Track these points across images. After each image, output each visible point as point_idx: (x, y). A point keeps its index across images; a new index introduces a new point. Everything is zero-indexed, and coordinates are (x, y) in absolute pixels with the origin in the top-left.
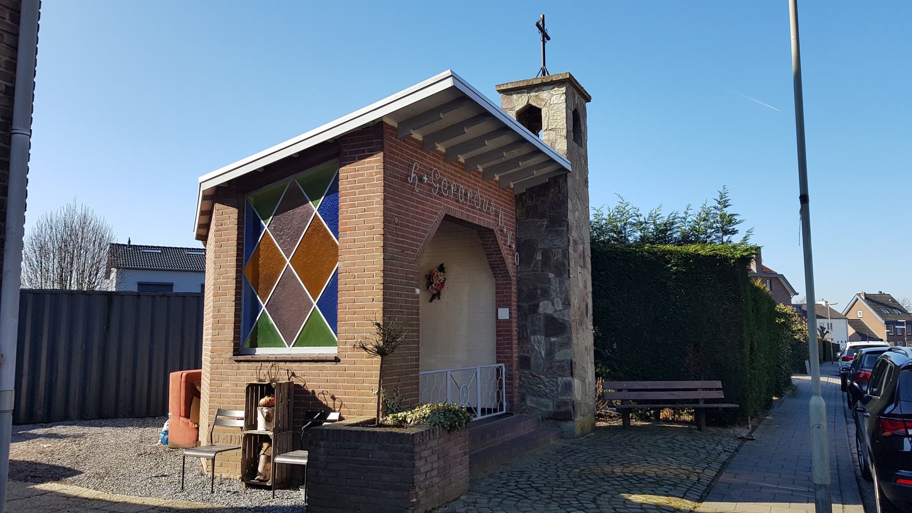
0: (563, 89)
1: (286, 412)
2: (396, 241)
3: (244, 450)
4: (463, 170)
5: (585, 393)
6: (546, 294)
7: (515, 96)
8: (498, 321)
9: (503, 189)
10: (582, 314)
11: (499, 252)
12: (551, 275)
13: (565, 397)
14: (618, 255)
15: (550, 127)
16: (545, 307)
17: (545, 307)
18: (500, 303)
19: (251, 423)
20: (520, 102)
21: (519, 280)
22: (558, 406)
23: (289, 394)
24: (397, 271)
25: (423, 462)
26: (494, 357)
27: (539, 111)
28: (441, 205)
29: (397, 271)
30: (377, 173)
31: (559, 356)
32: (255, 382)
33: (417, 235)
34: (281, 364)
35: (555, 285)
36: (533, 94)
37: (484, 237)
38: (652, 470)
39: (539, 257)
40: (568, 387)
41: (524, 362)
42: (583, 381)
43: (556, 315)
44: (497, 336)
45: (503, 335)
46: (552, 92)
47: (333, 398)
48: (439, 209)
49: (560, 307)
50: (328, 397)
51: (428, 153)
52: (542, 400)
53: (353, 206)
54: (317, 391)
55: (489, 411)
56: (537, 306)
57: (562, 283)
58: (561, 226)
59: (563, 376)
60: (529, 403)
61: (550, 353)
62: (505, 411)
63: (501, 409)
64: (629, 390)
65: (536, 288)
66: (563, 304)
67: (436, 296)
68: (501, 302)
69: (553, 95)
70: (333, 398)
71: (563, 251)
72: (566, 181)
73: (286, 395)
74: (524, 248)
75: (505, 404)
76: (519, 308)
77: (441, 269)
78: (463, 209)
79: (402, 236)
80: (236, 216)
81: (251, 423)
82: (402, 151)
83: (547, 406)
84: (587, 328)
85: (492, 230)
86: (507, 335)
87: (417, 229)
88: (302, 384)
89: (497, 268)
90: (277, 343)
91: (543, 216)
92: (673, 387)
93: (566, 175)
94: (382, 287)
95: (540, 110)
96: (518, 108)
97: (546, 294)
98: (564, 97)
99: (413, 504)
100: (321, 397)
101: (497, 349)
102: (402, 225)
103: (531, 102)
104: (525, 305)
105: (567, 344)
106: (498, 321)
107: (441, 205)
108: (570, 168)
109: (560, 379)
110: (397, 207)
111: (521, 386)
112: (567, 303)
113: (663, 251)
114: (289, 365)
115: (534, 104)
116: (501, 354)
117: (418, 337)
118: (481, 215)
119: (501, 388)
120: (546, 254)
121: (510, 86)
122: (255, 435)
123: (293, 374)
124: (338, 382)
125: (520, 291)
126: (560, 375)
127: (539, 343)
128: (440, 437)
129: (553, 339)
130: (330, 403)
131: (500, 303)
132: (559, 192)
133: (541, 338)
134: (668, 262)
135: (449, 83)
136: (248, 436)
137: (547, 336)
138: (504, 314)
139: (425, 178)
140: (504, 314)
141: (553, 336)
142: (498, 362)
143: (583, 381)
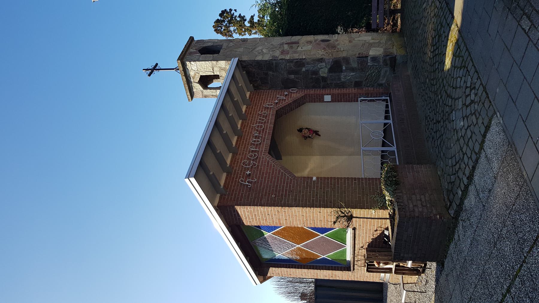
0: (188, 63)
1: (383, 253)
2: (285, 196)
3: (404, 274)
4: (241, 137)
5: (379, 44)
6: (316, 73)
7: (194, 90)
8: (332, 101)
9: (251, 101)
10: (328, 46)
11: (289, 105)
12: (304, 69)
15: (212, 70)
16: (324, 72)
17: (324, 72)
18: (321, 100)
19: (389, 270)
21: (307, 87)
22: (387, 65)
23: (373, 251)
24: (303, 196)
25: (416, 210)
26: (353, 104)
27: (202, 77)
28: (263, 158)
29: (303, 196)
30: (247, 209)
31: (355, 65)
32: (366, 268)
33: (281, 178)
34: (356, 252)
35: (310, 67)
36: (192, 80)
37: (281, 114)
38: (430, 33)
39: (292, 76)
40: (374, 59)
42: (371, 45)
43: (329, 67)
44: (341, 102)
45: (341, 98)
46: (190, 69)
47: (376, 230)
48: (266, 160)
49: (324, 64)
50: (375, 233)
51: (233, 168)
52: (382, 74)
53: (266, 220)
54: (372, 237)
55: (387, 112)
56: (323, 77)
57: (308, 64)
58: (273, 64)
59: (367, 62)
60: (384, 82)
61: (353, 70)
62: (388, 98)
63: (386, 101)
64: (378, 9)
66: (321, 62)
67: (317, 133)
68: (321, 99)
69: (192, 69)
70: (376, 230)
72: (244, 61)
73: (374, 253)
74: (287, 85)
75: (383, 98)
76: (324, 87)
77: (300, 130)
78: (264, 138)
79: (283, 192)
80: (274, 269)
81: (389, 270)
82: (233, 191)
83: (386, 71)
84: (337, 40)
85: (277, 111)
86: (341, 96)
87: (278, 177)
88: (367, 244)
89: (299, 103)
90: (344, 252)
94: (312, 208)
95: (201, 76)
96: (202, 89)
97: (316, 73)
98: (192, 63)
99: (440, 218)
100: (375, 236)
101: (349, 101)
102: (276, 190)
103: (197, 81)
104: (322, 84)
105: (346, 60)
106: (332, 101)
107: (263, 158)
108: (236, 59)
109: (369, 64)
110: (265, 195)
111: (373, 86)
112: (321, 60)
114: (356, 249)
115: (198, 79)
116: (354, 99)
117: (341, 178)
118: (268, 122)
119: (373, 101)
120: (291, 72)
121: (189, 94)
122: (395, 269)
123: (362, 247)
124: (367, 228)
125: (314, 87)
126: (367, 64)
127: (346, 76)
128: (402, 192)
129: (344, 68)
130: (379, 232)
131: (321, 100)
133: (342, 75)
135: (193, 180)
136: (396, 273)
137: (342, 71)
138: (327, 98)
139: (248, 172)
140: (327, 98)
141: (342, 69)
142: (357, 101)
143: (371, 45)
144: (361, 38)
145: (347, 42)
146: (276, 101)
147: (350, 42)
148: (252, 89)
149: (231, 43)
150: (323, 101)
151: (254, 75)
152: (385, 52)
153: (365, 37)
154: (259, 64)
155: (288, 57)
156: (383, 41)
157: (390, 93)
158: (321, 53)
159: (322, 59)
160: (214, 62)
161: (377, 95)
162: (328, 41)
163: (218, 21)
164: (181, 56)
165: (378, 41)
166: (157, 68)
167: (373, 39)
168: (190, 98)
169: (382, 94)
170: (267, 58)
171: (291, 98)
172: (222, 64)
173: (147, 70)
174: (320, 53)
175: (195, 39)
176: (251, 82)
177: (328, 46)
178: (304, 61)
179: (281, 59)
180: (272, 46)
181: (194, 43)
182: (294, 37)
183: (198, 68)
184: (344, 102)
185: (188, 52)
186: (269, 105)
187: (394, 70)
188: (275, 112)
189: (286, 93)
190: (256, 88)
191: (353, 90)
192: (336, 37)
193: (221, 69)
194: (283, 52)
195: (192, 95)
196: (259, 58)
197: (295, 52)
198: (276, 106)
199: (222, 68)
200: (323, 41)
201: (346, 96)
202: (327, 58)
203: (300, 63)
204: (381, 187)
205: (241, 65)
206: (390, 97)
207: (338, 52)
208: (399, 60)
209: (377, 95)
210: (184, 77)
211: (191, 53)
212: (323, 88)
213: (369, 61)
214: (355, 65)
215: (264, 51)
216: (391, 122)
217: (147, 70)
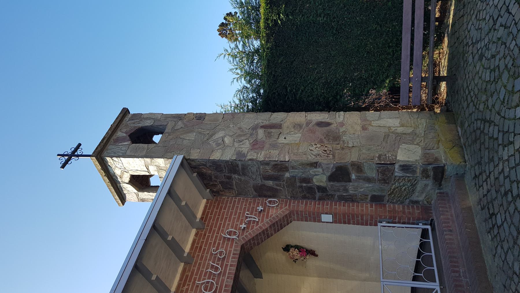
0: (108, 159)
5: (411, 138)
8: (335, 222)
12: (287, 175)
13: (418, 171)
14: (271, 73)
17: (320, 179)
20: (129, 190)
22: (427, 177)
31: (372, 174)
35: (298, 173)
36: (120, 180)
39: (270, 183)
40: (406, 168)
41: (376, 199)
46: (113, 167)
49: (320, 170)
57: (293, 168)
58: (237, 166)
60: (420, 199)
61: (368, 180)
62: (429, 227)
65: (301, 187)
66: (316, 167)
67: (313, 253)
68: (317, 219)
71: (263, 165)
72: (193, 160)
74: (262, 192)
77: (287, 248)
84: (342, 124)
86: (348, 216)
91: (229, 178)
92: (410, 6)
93: (187, 160)
96: (136, 191)
97: (307, 180)
98: (115, 159)
104: (318, 195)
105: (358, 167)
108: (180, 158)
112: (315, 165)
113: (265, 28)
132: (205, 165)
133: (351, 187)
134: (276, 22)
137: (350, 180)
140: (327, 218)
143: (401, 138)
144: (382, 122)
145: (359, 128)
146: (243, 226)
147: (364, 128)
148: (210, 196)
149: (180, 123)
150: (320, 221)
151: (212, 178)
152: (425, 155)
153: (390, 121)
154: (217, 165)
155: (261, 156)
156: (421, 130)
157: (432, 220)
158: (315, 152)
159: (316, 163)
160: (148, 160)
161: (409, 219)
162: (328, 124)
163: (222, 25)
164: (99, 149)
165: (410, 130)
166: (79, 152)
167: (402, 126)
168: (120, 202)
169: (419, 219)
170: (228, 155)
171: (267, 218)
172: (161, 162)
173: (63, 155)
174: (311, 151)
175: (132, 112)
176: (207, 186)
177: (327, 136)
178: (287, 165)
179: (250, 160)
180: (239, 132)
181: (127, 119)
182: (275, 115)
183: (127, 166)
184: (354, 224)
185: (114, 137)
186: (230, 233)
187: (440, 185)
188: (239, 249)
189: (260, 208)
190: (215, 193)
191: (368, 209)
192: (342, 117)
193: (159, 168)
194: (256, 145)
195: (122, 198)
196: (216, 156)
197: (274, 146)
198: (243, 234)
199: (159, 169)
200: (320, 124)
201: (357, 217)
202: (325, 162)
203: (281, 167)
204: (384, 81)
205: (188, 165)
206: (432, 224)
207: (343, 149)
208: (449, 171)
209: (409, 219)
210: (106, 178)
211: (118, 140)
212: (320, 199)
213: (396, 170)
214: (372, 174)
215: (227, 140)
216: (438, 288)
217: (63, 155)
